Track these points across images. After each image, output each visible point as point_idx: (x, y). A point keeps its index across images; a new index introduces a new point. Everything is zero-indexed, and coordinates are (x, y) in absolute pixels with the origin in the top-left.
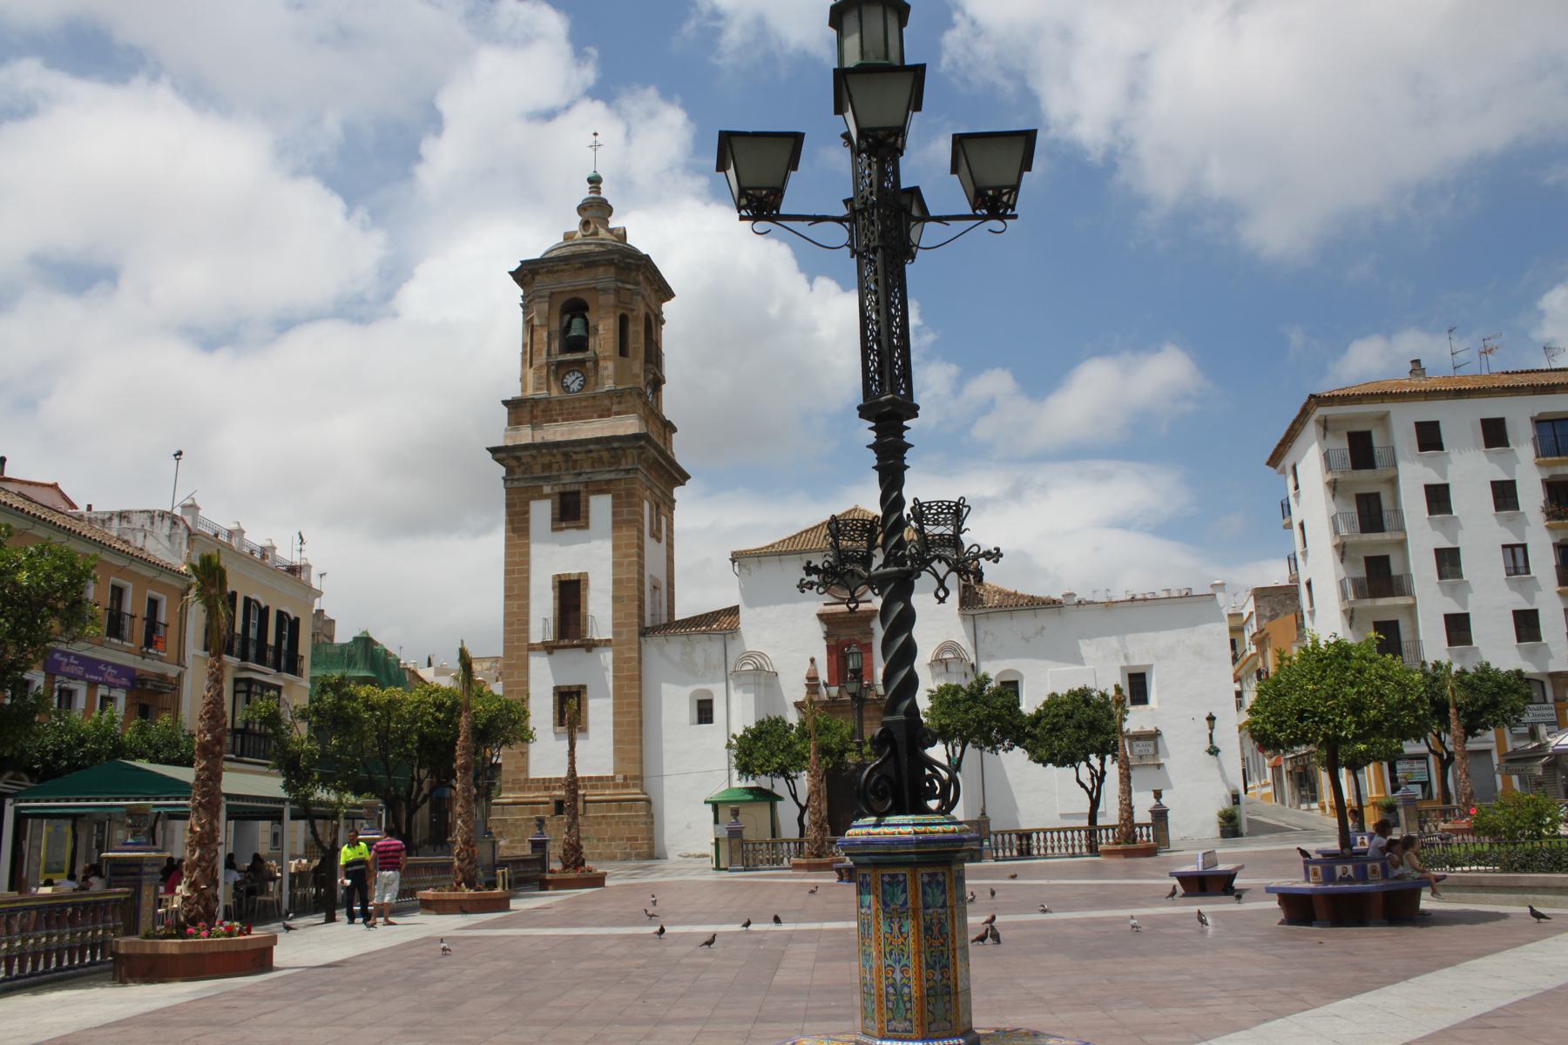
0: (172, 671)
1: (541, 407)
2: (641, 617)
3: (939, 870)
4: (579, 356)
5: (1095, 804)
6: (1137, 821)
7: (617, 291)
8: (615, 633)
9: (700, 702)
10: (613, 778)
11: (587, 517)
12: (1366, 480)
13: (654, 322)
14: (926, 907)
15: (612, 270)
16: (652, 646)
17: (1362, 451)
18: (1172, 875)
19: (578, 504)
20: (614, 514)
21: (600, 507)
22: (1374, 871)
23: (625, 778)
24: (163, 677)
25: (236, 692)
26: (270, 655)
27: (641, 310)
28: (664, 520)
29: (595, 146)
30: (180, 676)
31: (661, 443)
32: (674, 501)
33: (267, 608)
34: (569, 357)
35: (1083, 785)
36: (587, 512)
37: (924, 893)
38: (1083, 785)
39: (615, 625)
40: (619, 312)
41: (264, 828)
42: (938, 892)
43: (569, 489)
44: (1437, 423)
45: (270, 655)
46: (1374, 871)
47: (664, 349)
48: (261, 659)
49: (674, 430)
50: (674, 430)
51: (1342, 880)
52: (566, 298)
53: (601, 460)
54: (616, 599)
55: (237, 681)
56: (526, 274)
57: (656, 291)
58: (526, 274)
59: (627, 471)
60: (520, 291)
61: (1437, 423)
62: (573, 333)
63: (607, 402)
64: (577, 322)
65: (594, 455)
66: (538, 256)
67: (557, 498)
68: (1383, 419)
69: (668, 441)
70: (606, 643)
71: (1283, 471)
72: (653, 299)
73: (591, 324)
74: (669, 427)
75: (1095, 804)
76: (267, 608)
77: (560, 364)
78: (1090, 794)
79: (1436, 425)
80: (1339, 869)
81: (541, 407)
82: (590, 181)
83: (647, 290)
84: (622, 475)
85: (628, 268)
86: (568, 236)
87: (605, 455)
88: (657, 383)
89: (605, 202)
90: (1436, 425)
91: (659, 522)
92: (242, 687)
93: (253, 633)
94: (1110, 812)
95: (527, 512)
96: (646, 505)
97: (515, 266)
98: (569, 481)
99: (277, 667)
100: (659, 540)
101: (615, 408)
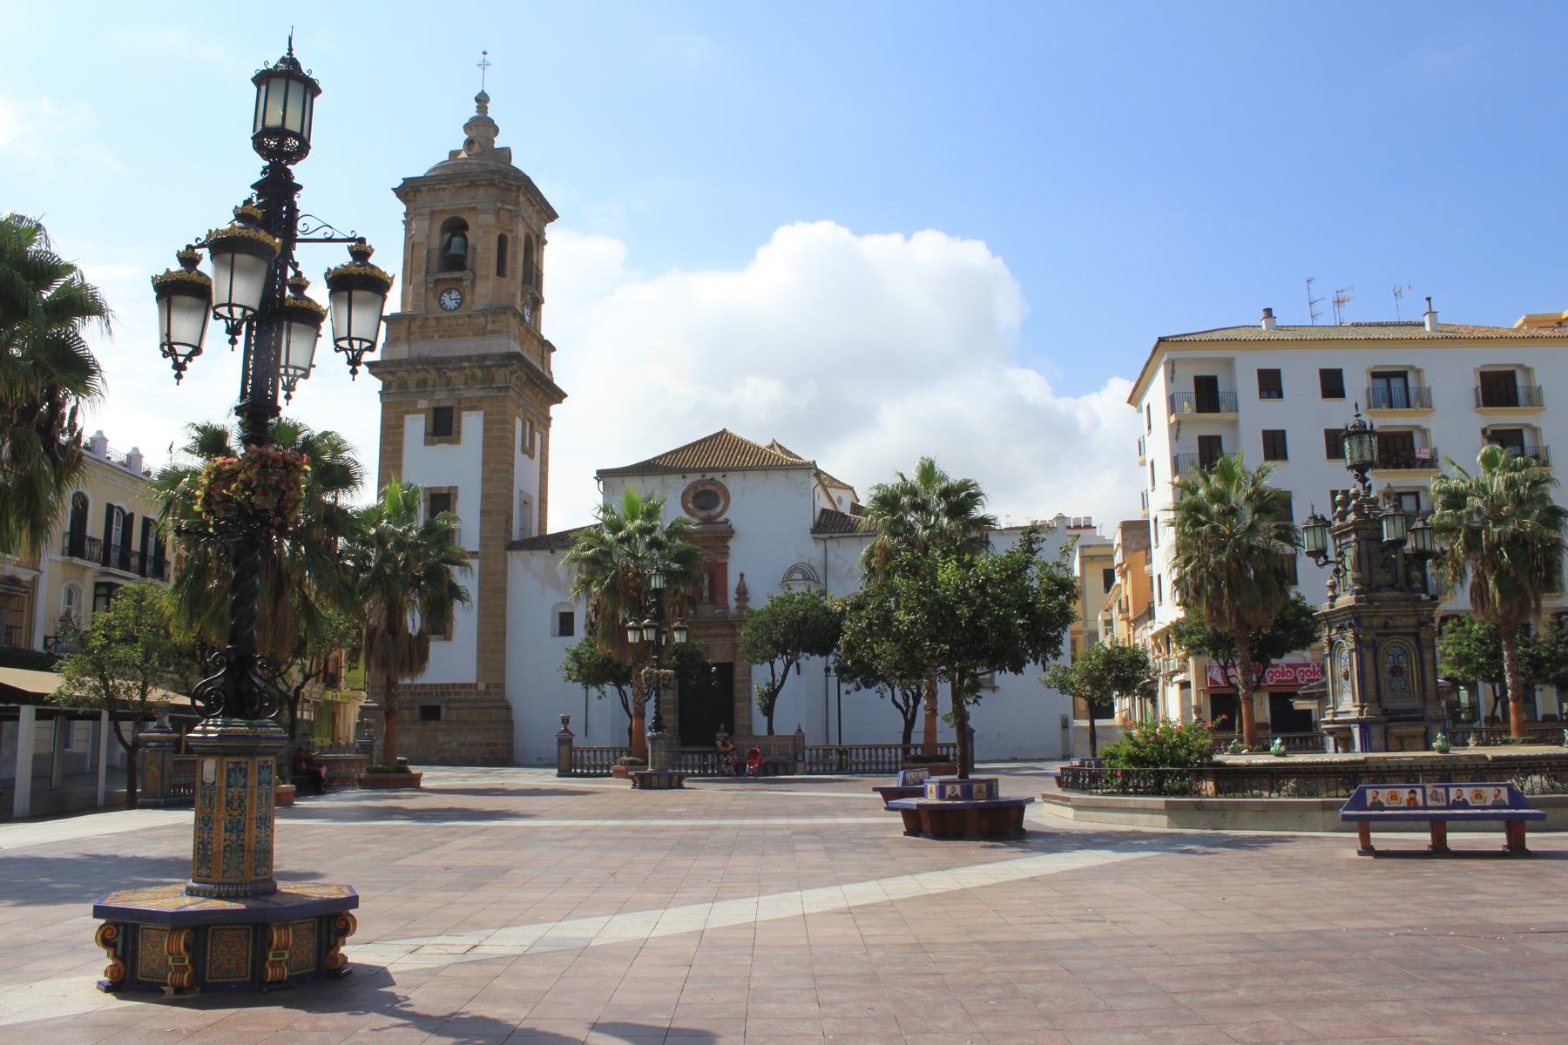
0: (25, 575)
1: (418, 323)
2: (509, 532)
3: (243, 759)
4: (456, 275)
5: (909, 724)
6: (940, 740)
7: (497, 212)
8: (481, 546)
9: (562, 615)
10: (476, 685)
11: (459, 433)
12: (1210, 424)
13: (535, 243)
14: (229, 786)
15: (493, 191)
16: (516, 560)
17: (1207, 394)
18: (875, 790)
19: (451, 418)
20: (485, 430)
21: (472, 425)
22: (980, 791)
23: (487, 686)
24: (13, 581)
25: (96, 596)
26: (135, 561)
27: (521, 232)
28: (538, 437)
29: (484, 65)
30: (35, 581)
31: (536, 364)
32: (549, 419)
33: (132, 515)
34: (447, 275)
35: (898, 706)
36: (459, 427)
37: (229, 776)
38: (898, 706)
39: (482, 539)
40: (498, 233)
41: (81, 729)
42: (240, 776)
43: (442, 404)
44: (1278, 372)
45: (135, 561)
46: (980, 791)
47: (545, 271)
48: (124, 564)
49: (553, 349)
50: (553, 349)
51: (950, 798)
52: (446, 217)
53: (474, 377)
54: (483, 513)
55: (98, 585)
56: (408, 190)
57: (539, 212)
58: (408, 190)
59: (500, 389)
60: (403, 208)
61: (1278, 372)
62: (452, 251)
63: (482, 320)
64: (456, 240)
65: (468, 372)
66: (421, 173)
67: (431, 413)
68: (1230, 363)
69: (545, 361)
70: (474, 554)
71: (1140, 411)
72: (534, 221)
73: (470, 242)
74: (548, 347)
75: (909, 724)
76: (132, 515)
77: (438, 281)
78: (905, 714)
79: (1277, 373)
80: (949, 789)
81: (418, 323)
82: (477, 99)
83: (527, 210)
84: (494, 393)
85: (508, 188)
86: (454, 154)
87: (479, 373)
88: (537, 302)
89: (491, 121)
90: (1277, 373)
91: (532, 439)
92: (103, 591)
93: (116, 538)
94: (918, 737)
95: (401, 426)
96: (518, 422)
97: (398, 183)
98: (442, 398)
99: (143, 573)
100: (532, 457)
101: (489, 327)
